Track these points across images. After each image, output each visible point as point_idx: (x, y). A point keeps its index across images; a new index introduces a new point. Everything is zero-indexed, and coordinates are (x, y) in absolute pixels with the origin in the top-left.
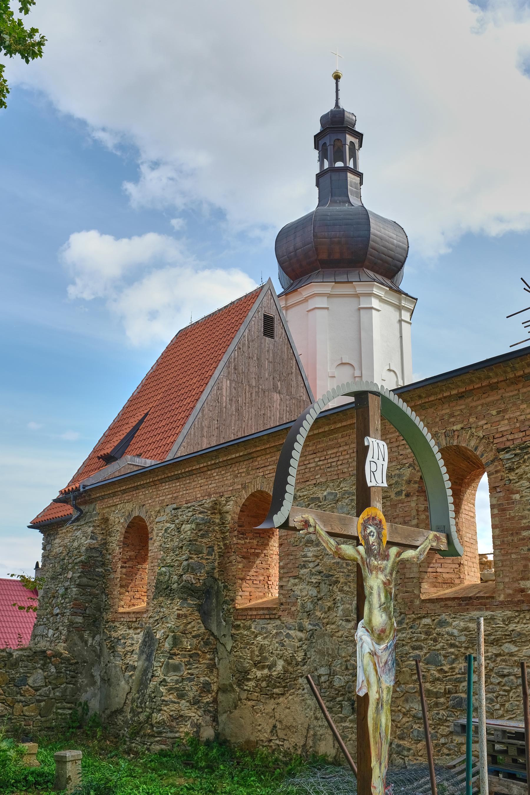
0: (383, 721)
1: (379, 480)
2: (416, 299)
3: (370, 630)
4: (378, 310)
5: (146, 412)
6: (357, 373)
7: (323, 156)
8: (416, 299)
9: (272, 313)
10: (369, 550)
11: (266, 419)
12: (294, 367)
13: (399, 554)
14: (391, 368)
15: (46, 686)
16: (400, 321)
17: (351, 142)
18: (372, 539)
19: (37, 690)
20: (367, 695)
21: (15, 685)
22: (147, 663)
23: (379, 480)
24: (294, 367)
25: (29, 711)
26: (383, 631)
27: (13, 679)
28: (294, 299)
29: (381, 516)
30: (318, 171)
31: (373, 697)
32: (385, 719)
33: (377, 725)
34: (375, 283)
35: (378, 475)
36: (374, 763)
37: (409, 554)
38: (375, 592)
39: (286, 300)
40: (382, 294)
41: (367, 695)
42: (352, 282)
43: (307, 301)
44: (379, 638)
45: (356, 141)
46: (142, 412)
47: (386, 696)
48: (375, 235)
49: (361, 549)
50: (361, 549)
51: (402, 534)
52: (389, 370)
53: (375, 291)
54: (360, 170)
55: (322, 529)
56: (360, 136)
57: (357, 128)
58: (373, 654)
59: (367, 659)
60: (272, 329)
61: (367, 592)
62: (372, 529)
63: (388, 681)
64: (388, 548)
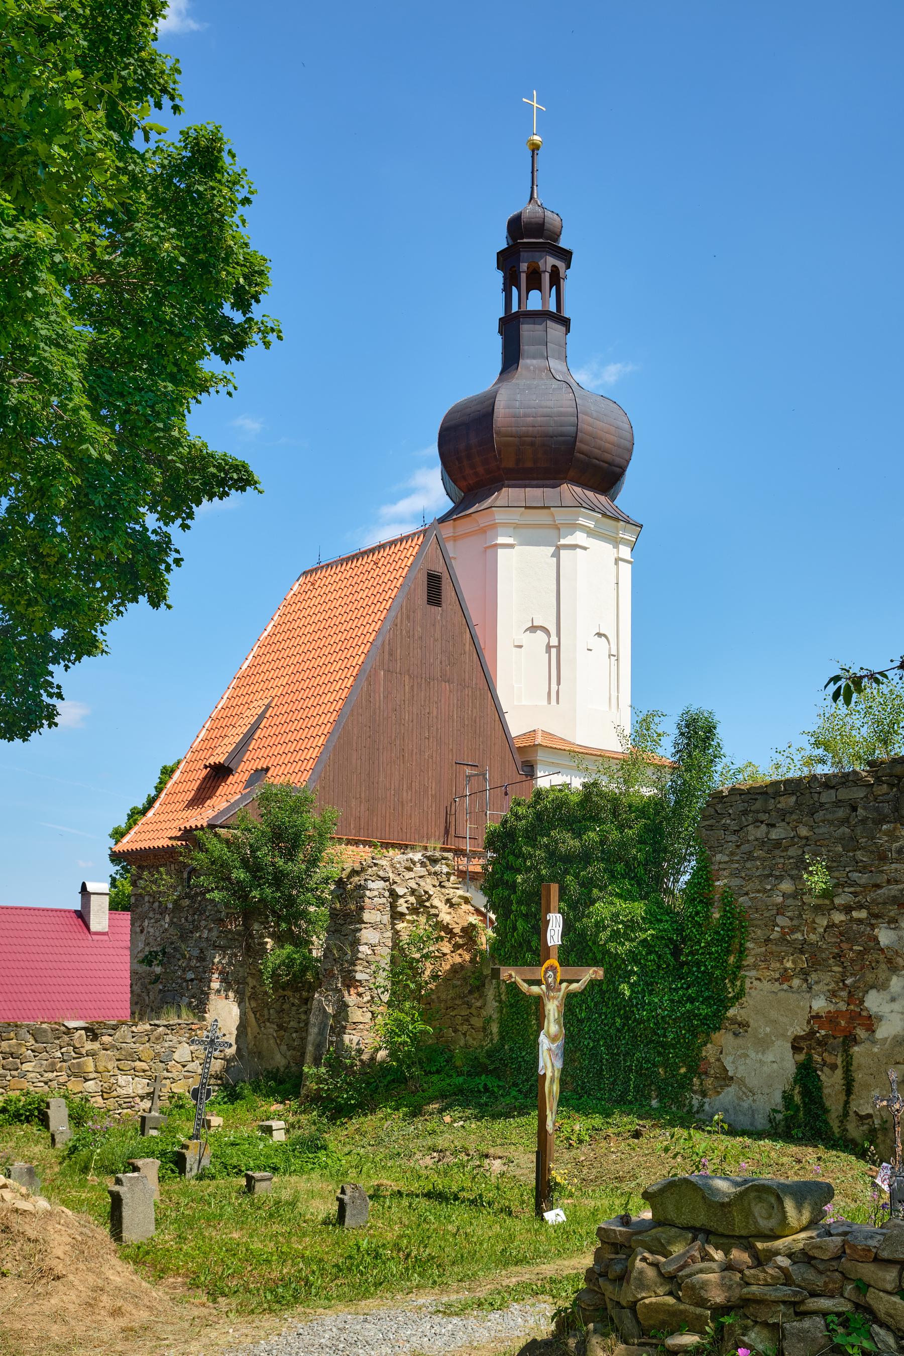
0: (555, 1089)
1: (556, 940)
2: (641, 526)
3: (548, 1035)
4: (585, 548)
5: (266, 702)
6: (554, 641)
7: (511, 281)
8: (641, 526)
9: (440, 568)
10: (548, 986)
11: (431, 719)
12: (467, 645)
13: (568, 987)
14: (601, 632)
15: (193, 1061)
16: (617, 560)
17: (554, 266)
18: (550, 980)
19: (184, 1066)
20: (545, 1074)
21: (161, 1062)
22: (320, 1037)
23: (556, 940)
24: (467, 645)
25: (178, 1088)
26: (556, 1036)
27: (158, 1054)
28: (464, 526)
29: (557, 964)
30: (502, 315)
31: (549, 1074)
32: (556, 1088)
33: (550, 1091)
34: (582, 509)
35: (555, 938)
36: (548, 1112)
37: (574, 986)
38: (551, 1013)
39: (454, 527)
40: (591, 524)
41: (545, 1074)
42: (549, 508)
43: (485, 532)
44: (553, 1039)
45: (560, 265)
46: (260, 703)
47: (557, 1074)
48: (584, 447)
49: (543, 987)
50: (543, 987)
51: (572, 972)
52: (599, 635)
53: (582, 521)
54: (566, 313)
55: (519, 980)
56: (566, 256)
57: (563, 243)
58: (549, 1050)
59: (546, 1053)
60: (439, 594)
61: (546, 1013)
62: (550, 973)
63: (559, 1064)
64: (560, 983)
